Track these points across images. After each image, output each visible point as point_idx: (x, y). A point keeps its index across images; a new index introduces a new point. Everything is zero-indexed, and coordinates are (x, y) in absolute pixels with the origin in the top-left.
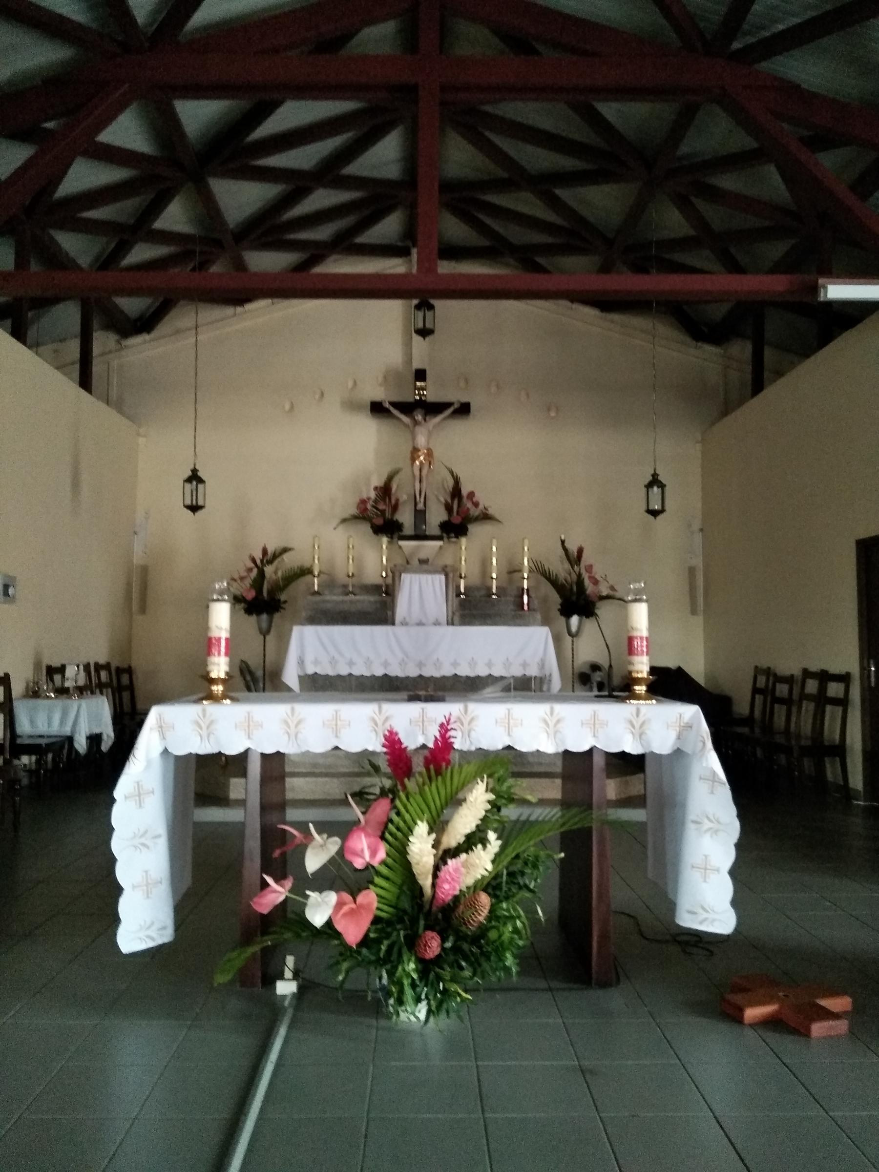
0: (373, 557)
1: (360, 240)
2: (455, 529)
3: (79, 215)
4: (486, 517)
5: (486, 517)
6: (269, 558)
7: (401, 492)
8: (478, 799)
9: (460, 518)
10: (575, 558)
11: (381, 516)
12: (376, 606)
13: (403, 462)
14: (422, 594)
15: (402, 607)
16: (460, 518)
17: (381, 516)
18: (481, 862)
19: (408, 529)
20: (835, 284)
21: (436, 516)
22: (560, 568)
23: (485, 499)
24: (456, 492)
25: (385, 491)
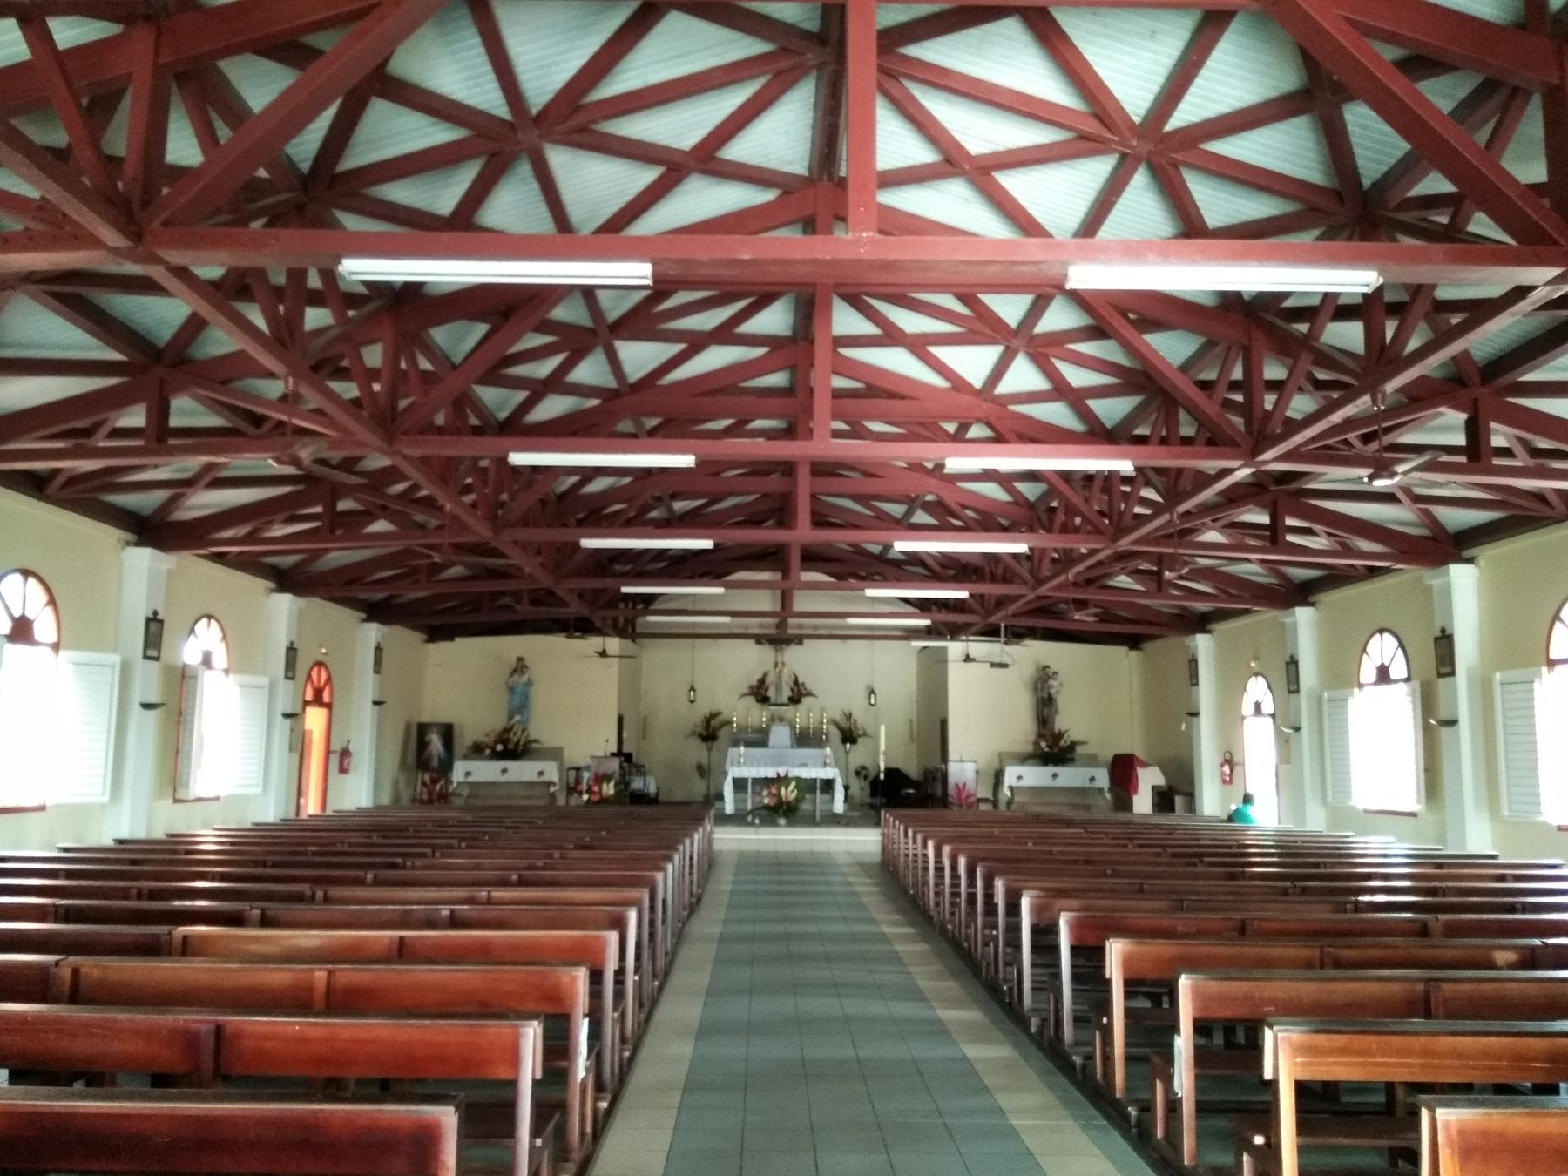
0: (757, 715)
1: (766, 196)
2: (795, 700)
3: (1054, 361)
4: (810, 694)
5: (810, 694)
6: (713, 716)
7: (770, 679)
8: (793, 784)
9: (798, 694)
10: (849, 717)
11: (760, 693)
12: (759, 739)
13: (770, 667)
14: (780, 735)
15: (773, 740)
16: (798, 694)
17: (760, 693)
18: (794, 795)
19: (773, 700)
20: (1163, 360)
21: (786, 693)
22: (844, 724)
23: (810, 686)
24: (796, 682)
25: (762, 682)
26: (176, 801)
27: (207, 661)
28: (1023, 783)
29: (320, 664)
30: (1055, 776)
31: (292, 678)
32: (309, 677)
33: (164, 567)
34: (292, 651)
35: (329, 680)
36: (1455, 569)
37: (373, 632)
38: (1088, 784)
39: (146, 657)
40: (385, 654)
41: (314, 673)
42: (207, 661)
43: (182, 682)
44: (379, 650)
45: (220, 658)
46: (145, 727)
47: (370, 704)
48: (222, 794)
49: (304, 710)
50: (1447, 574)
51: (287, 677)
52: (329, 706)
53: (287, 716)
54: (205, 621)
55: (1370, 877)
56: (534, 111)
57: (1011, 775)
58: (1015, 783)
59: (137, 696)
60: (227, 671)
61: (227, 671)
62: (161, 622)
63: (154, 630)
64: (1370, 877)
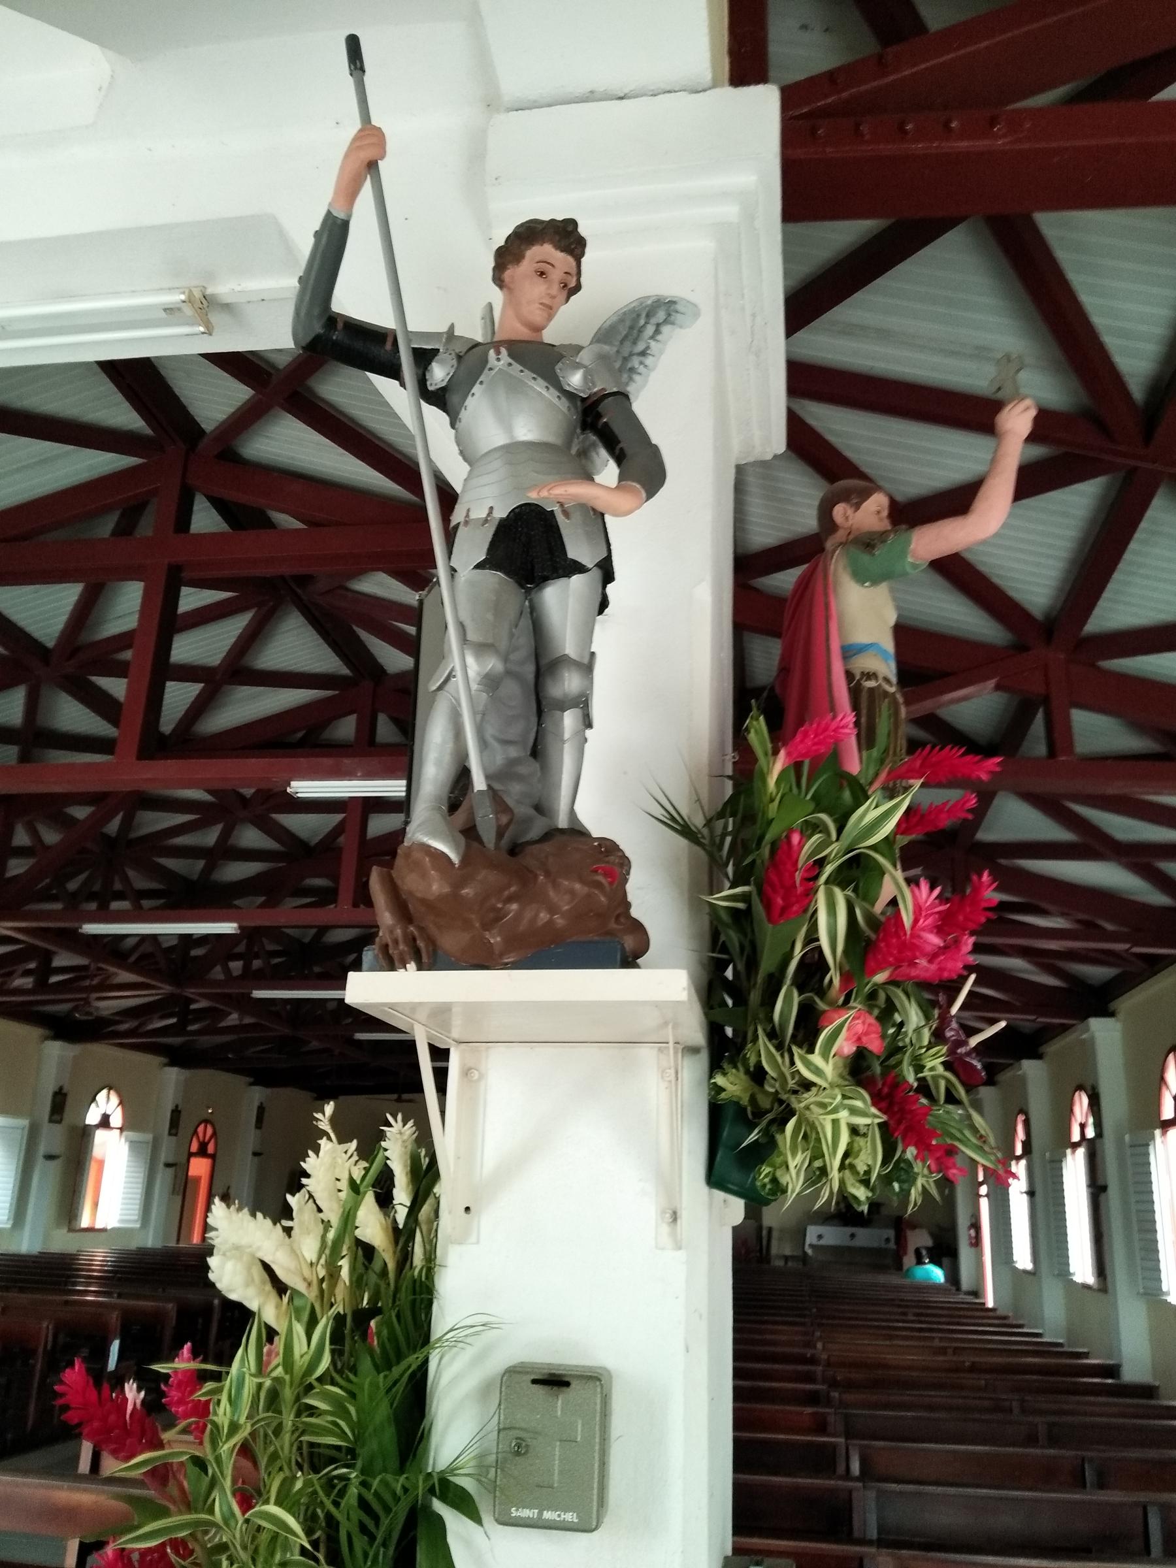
26: (71, 1230)
27: (105, 1122)
28: (822, 1242)
29: (206, 1121)
30: (853, 1236)
31: (176, 1135)
32: (195, 1132)
33: (72, 1054)
34: (176, 1113)
35: (214, 1134)
36: (1097, 1025)
37: (257, 1095)
38: (883, 1245)
39: (51, 1121)
40: (266, 1114)
41: (201, 1129)
42: (105, 1122)
43: (83, 1136)
44: (261, 1110)
45: (116, 1120)
46: (46, 1177)
47: (250, 1156)
48: (109, 1227)
49: (188, 1161)
50: (1087, 1030)
51: (170, 1134)
52: (213, 1157)
53: (168, 1165)
54: (105, 1092)
55: (83, 1270)
56: (1137, 390)
57: (813, 1234)
58: (815, 1242)
59: (42, 1149)
60: (121, 1129)
61: (121, 1129)
62: (65, 1095)
63: (59, 1103)
64: (83, 1270)
